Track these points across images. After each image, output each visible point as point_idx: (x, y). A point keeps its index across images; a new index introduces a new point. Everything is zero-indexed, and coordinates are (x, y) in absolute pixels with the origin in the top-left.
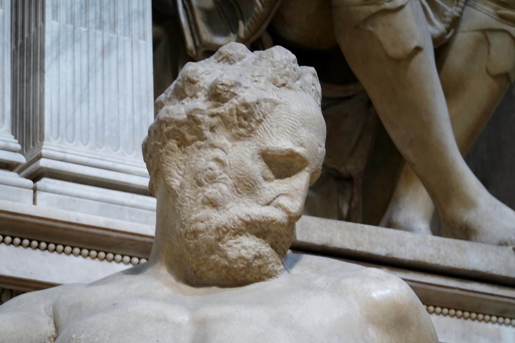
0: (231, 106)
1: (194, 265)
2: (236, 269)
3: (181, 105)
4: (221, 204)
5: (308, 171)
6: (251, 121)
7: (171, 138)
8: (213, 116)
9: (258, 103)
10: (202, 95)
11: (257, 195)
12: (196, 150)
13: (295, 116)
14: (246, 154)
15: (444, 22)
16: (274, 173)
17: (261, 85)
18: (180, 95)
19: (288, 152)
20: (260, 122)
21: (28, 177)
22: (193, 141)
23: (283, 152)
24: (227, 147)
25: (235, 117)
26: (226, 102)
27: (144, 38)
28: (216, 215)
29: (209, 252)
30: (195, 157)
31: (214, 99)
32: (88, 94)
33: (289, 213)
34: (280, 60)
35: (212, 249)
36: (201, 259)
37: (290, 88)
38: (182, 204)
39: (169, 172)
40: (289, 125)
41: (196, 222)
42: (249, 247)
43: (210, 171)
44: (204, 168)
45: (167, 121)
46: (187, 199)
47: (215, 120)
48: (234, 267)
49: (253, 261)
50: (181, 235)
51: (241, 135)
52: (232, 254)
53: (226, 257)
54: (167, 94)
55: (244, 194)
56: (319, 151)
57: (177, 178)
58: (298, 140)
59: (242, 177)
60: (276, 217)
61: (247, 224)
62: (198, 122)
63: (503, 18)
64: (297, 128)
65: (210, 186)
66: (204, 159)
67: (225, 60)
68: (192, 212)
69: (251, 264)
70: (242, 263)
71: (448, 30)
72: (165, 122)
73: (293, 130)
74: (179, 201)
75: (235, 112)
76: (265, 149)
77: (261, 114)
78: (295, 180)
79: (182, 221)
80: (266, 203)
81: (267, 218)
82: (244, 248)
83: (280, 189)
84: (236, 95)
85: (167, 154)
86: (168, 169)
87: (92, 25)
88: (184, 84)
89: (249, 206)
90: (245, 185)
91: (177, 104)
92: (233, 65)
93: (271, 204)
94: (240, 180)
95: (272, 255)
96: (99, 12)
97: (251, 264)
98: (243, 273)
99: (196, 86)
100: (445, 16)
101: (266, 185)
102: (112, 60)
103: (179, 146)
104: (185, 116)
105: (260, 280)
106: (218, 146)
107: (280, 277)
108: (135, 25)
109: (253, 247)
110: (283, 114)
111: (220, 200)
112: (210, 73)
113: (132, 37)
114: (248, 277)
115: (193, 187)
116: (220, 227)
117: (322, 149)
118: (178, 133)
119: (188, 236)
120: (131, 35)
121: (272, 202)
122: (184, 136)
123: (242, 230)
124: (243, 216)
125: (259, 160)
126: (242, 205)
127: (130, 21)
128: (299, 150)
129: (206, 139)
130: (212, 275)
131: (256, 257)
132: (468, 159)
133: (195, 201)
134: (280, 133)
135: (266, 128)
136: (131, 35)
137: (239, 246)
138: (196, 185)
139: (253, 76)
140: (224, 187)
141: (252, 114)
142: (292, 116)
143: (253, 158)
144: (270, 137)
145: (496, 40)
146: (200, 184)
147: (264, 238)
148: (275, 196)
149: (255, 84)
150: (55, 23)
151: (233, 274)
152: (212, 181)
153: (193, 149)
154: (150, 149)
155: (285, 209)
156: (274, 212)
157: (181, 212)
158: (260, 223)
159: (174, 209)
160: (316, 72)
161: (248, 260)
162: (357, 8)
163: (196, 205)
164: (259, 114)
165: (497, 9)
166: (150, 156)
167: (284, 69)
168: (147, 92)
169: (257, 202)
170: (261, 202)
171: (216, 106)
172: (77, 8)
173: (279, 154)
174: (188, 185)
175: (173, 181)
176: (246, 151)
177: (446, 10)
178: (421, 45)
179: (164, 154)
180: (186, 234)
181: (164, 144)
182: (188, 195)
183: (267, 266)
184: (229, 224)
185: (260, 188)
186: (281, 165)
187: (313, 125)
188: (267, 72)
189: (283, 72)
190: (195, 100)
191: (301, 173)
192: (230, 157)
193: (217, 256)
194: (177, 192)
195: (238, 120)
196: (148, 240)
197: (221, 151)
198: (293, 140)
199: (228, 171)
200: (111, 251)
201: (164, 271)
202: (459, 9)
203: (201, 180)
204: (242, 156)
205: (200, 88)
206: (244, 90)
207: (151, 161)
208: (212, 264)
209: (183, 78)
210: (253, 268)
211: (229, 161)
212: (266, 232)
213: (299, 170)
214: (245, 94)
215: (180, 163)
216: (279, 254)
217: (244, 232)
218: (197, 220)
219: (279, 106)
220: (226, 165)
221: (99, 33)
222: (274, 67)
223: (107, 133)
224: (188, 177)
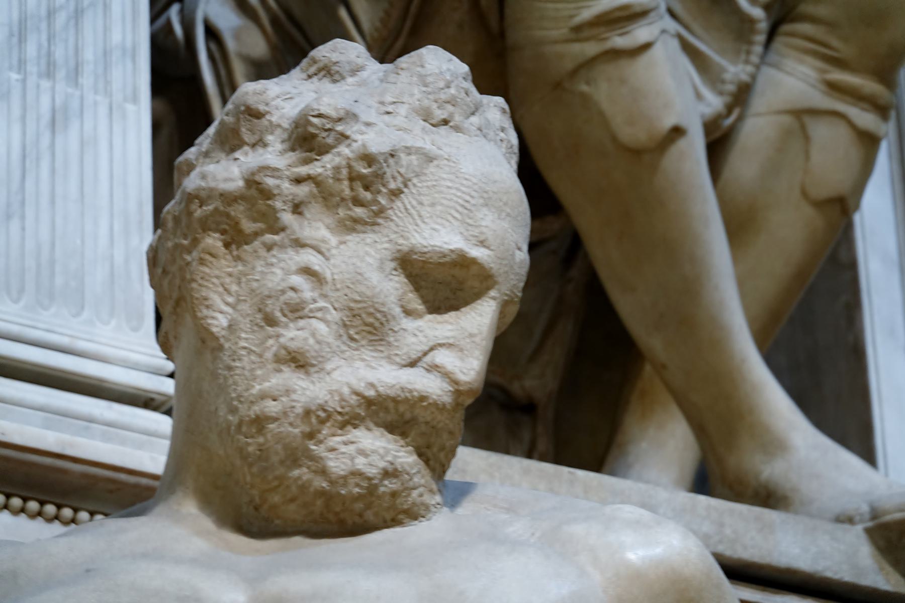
0: (337, 160)
1: (255, 492)
2: (343, 496)
3: (231, 162)
4: (314, 362)
5: (494, 298)
6: (379, 192)
7: (210, 230)
8: (298, 181)
9: (392, 156)
11: (389, 344)
12: (262, 252)
13: (470, 183)
14: (368, 259)
15: (721, 93)
16: (425, 302)
17: (399, 121)
18: (230, 142)
19: (454, 256)
20: (396, 194)
22: (257, 234)
23: (445, 256)
24: (327, 246)
25: (346, 183)
26: (327, 152)
27: (135, 100)
28: (304, 384)
29: (288, 463)
30: (259, 266)
31: (301, 147)
32: (23, 203)
33: (455, 382)
34: (437, 71)
35: (295, 456)
36: (270, 477)
37: (457, 129)
38: (233, 364)
39: (206, 299)
40: (457, 202)
41: (262, 399)
42: (373, 452)
43: (291, 294)
44: (280, 288)
45: (203, 194)
46: (243, 352)
47: (303, 190)
48: (339, 494)
49: (381, 480)
50: (229, 428)
51: (356, 221)
52: (337, 465)
53: (323, 472)
54: (200, 144)
55: (364, 342)
56: (517, 259)
57: (221, 312)
58: (476, 232)
59: (360, 306)
60: (430, 390)
61: (369, 403)
62: (267, 194)
63: (834, 88)
64: (473, 208)
65: (291, 325)
66: (279, 271)
67: (323, 73)
68: (255, 378)
69: (376, 487)
70: (357, 485)
71: (729, 109)
72: (197, 197)
73: (466, 211)
74: (225, 358)
75: (345, 172)
76: (405, 249)
77: (400, 179)
78: (468, 316)
79: (232, 399)
80: (409, 361)
81: (411, 391)
82: (362, 453)
83: (437, 333)
84: (347, 137)
85: (202, 262)
86: (204, 294)
88: (238, 120)
89: (373, 368)
90: (366, 325)
91: (224, 163)
92: (338, 84)
93: (419, 364)
94: (356, 312)
95: (418, 472)
96: (45, 44)
97: (376, 487)
98: (359, 506)
99: (264, 122)
100: (723, 82)
101: (408, 324)
102: (70, 140)
103: (227, 245)
104: (241, 183)
105: (394, 522)
106: (308, 242)
107: (434, 517)
108: (117, 74)
109: (381, 451)
110: (444, 179)
111: (314, 354)
112: (291, 98)
113: (111, 96)
114: (369, 516)
115: (256, 328)
116: (314, 408)
117: (521, 253)
118: (224, 219)
119: (244, 429)
120: (108, 93)
121: (419, 359)
122: (237, 223)
123: (357, 417)
124: (361, 387)
125: (394, 273)
126: (358, 364)
127: (107, 67)
128: (476, 252)
129: (283, 229)
130: (292, 511)
131: (387, 474)
132: (769, 360)
133: (260, 356)
134: (438, 217)
135: (409, 207)
136: (108, 93)
137: (351, 448)
138: (263, 324)
139: (382, 103)
140: (322, 327)
141: (379, 176)
142: (462, 185)
143: (381, 268)
144: (417, 225)
146: (271, 321)
147: (403, 435)
148: (426, 348)
149: (386, 117)
151: (338, 509)
152: (297, 315)
153: (256, 251)
154: (163, 257)
155: (447, 375)
156: (425, 381)
157: (231, 381)
158: (395, 400)
159: (215, 376)
160: (506, 107)
161: (370, 479)
162: (559, 48)
163: (262, 365)
164: (394, 178)
165: (823, 71)
166: (165, 272)
167: (446, 90)
168: (140, 205)
169: (389, 358)
170: (398, 359)
171: (307, 162)
173: (435, 259)
174: (245, 324)
175: (213, 318)
176: (367, 254)
177: (724, 70)
178: (683, 122)
179: (194, 264)
180: (240, 425)
181: (195, 242)
182: (246, 345)
183: (409, 495)
184: (331, 404)
185: (396, 329)
186: (441, 284)
187: (506, 204)
188: (412, 95)
189: (443, 97)
190: (260, 150)
191: (479, 301)
192: (334, 266)
193: (305, 470)
194: (222, 340)
195: (352, 189)
196: (144, 481)
197: (315, 253)
198: (466, 233)
199: (331, 294)
200: (69, 503)
201: (190, 507)
202: (750, 69)
203: (273, 313)
204: (359, 264)
205: (273, 127)
206: (363, 128)
207: (165, 283)
208: (294, 489)
209: (237, 107)
210: (379, 497)
211: (333, 274)
212: (407, 422)
213: (477, 296)
214: (365, 137)
215: (228, 280)
216: (433, 470)
217: (362, 419)
218: (263, 396)
219: (435, 162)
220: (327, 282)
221: (45, 84)
222: (426, 86)
223: (59, 281)
224: (245, 307)
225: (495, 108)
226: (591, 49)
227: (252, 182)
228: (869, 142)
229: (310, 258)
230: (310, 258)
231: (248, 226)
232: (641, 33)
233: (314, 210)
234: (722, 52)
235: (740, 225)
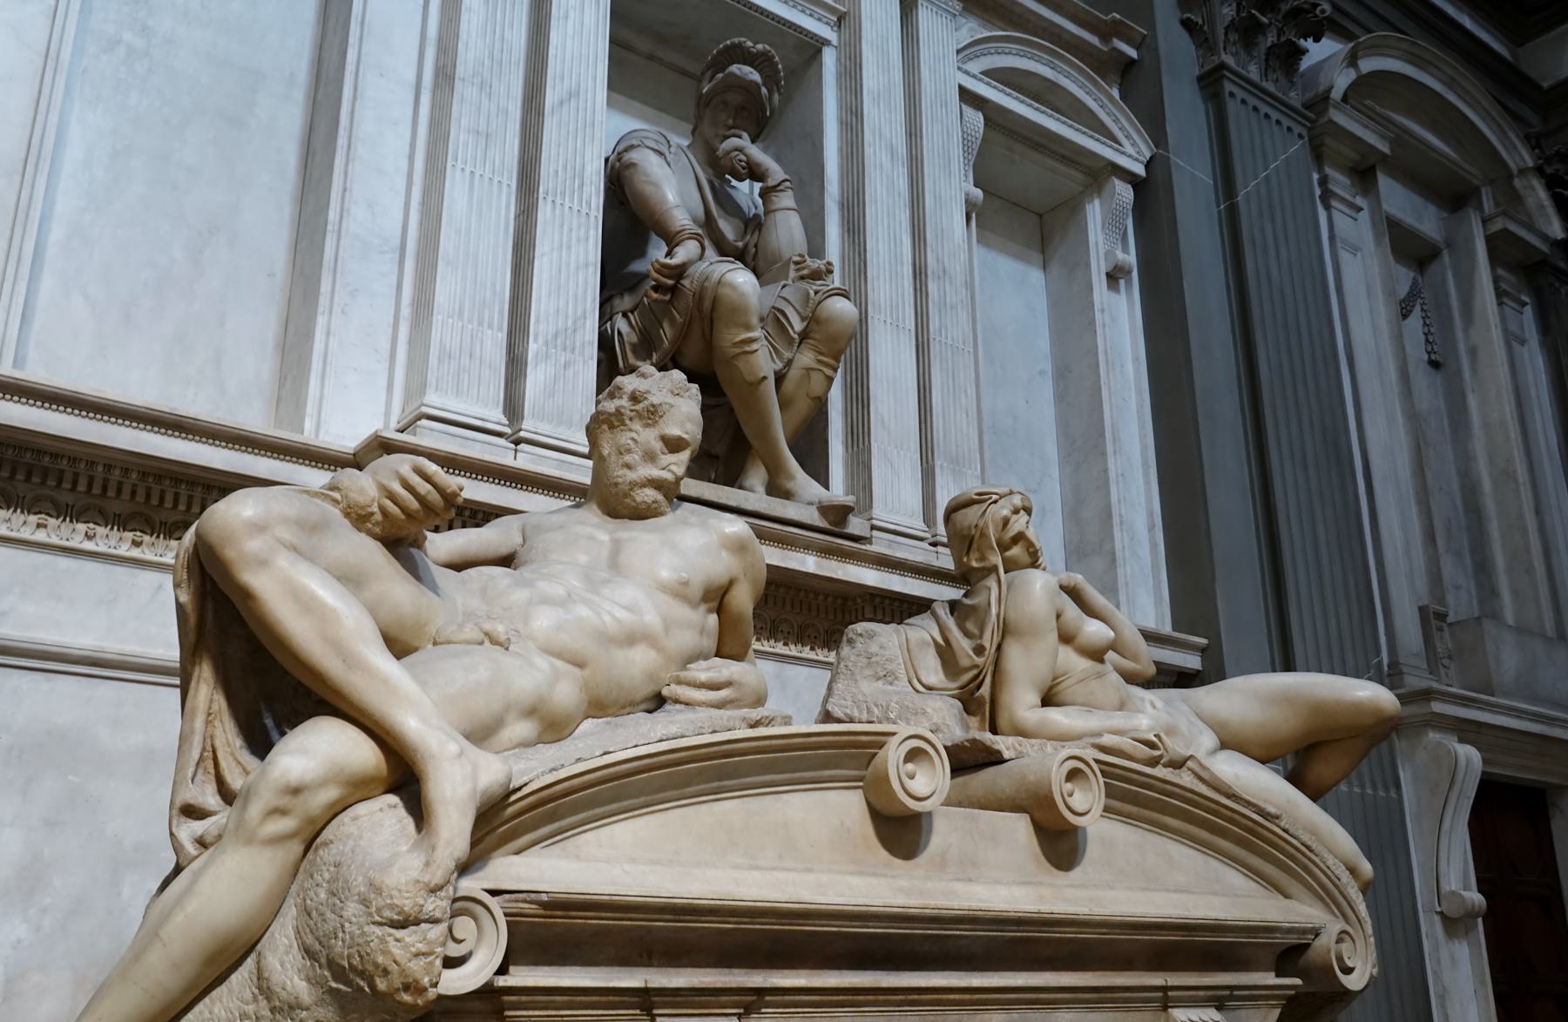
35: (626, 495)
63: (819, 361)
66: (624, 438)
102: (570, 372)
130: (625, 512)
186: (674, 445)
201: (595, 507)
225: (695, 388)
226: (738, 350)
227: (617, 410)
228: (830, 380)
230: (634, 435)
232: (755, 346)
233: (636, 420)
235: (784, 405)
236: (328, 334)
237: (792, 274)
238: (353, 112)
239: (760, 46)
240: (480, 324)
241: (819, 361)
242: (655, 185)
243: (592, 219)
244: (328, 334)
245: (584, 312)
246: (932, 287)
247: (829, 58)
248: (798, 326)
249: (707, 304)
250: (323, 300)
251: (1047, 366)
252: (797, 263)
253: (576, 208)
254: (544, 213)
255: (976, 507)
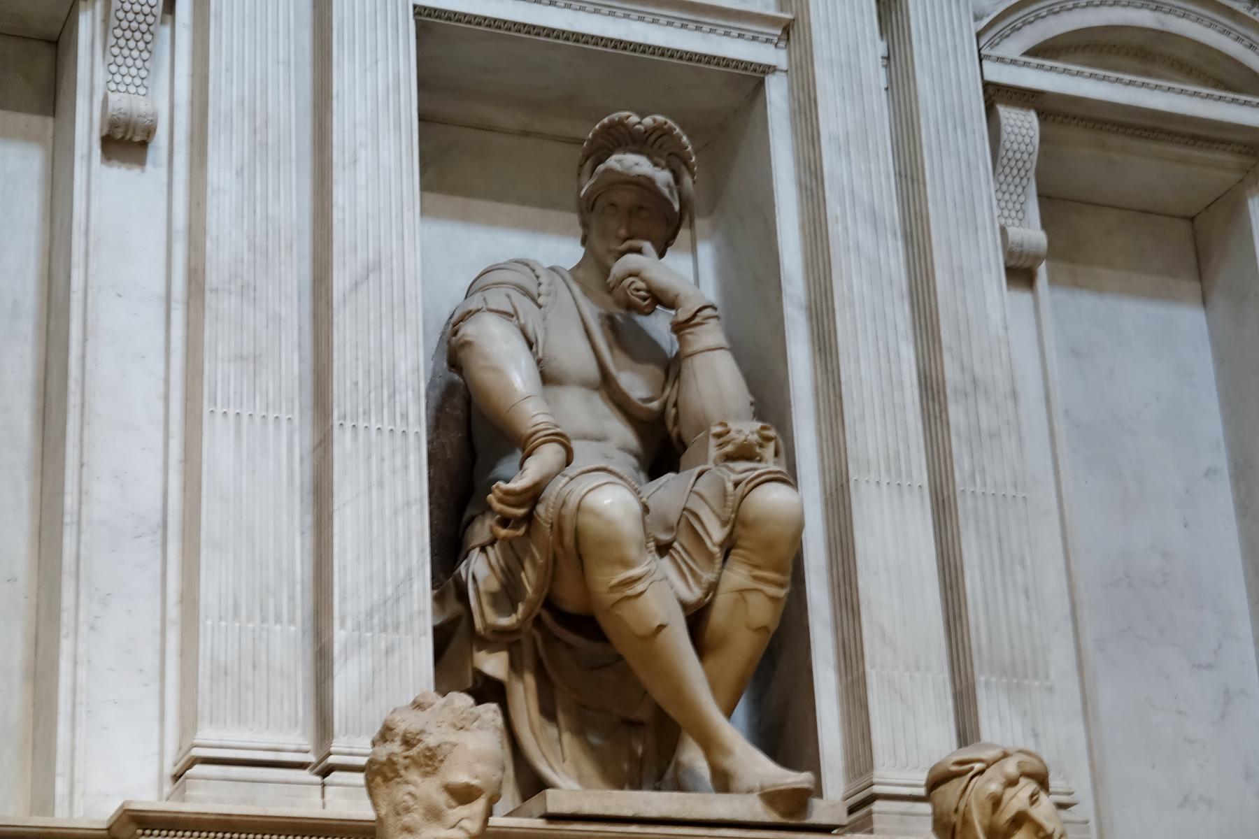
10: (398, 740)
20: (442, 761)
21: (318, 774)
22: (393, 778)
47: (408, 761)
63: (756, 578)
71: (706, 595)
87: (377, 629)
101: (451, 812)
128: (474, 782)
145: (753, 599)
146: (398, 814)
150: (343, 633)
155: (467, 831)
172: (362, 617)
205: (397, 735)
221: (383, 635)
226: (618, 596)
227: (389, 759)
229: (411, 788)
230: (411, 788)
231: (390, 775)
232: (639, 587)
234: (702, 569)
236: (75, 663)
237: (713, 452)
238: (83, 357)
239: (648, 121)
240: (264, 620)
241: (756, 578)
242: (496, 370)
243: (411, 437)
244: (75, 663)
245: (409, 571)
246: (955, 413)
247: (777, 92)
248: (717, 533)
249: (568, 539)
250: (66, 618)
251: (1220, 460)
252: (719, 436)
253: (387, 427)
254: (343, 444)
255: (955, 782)
